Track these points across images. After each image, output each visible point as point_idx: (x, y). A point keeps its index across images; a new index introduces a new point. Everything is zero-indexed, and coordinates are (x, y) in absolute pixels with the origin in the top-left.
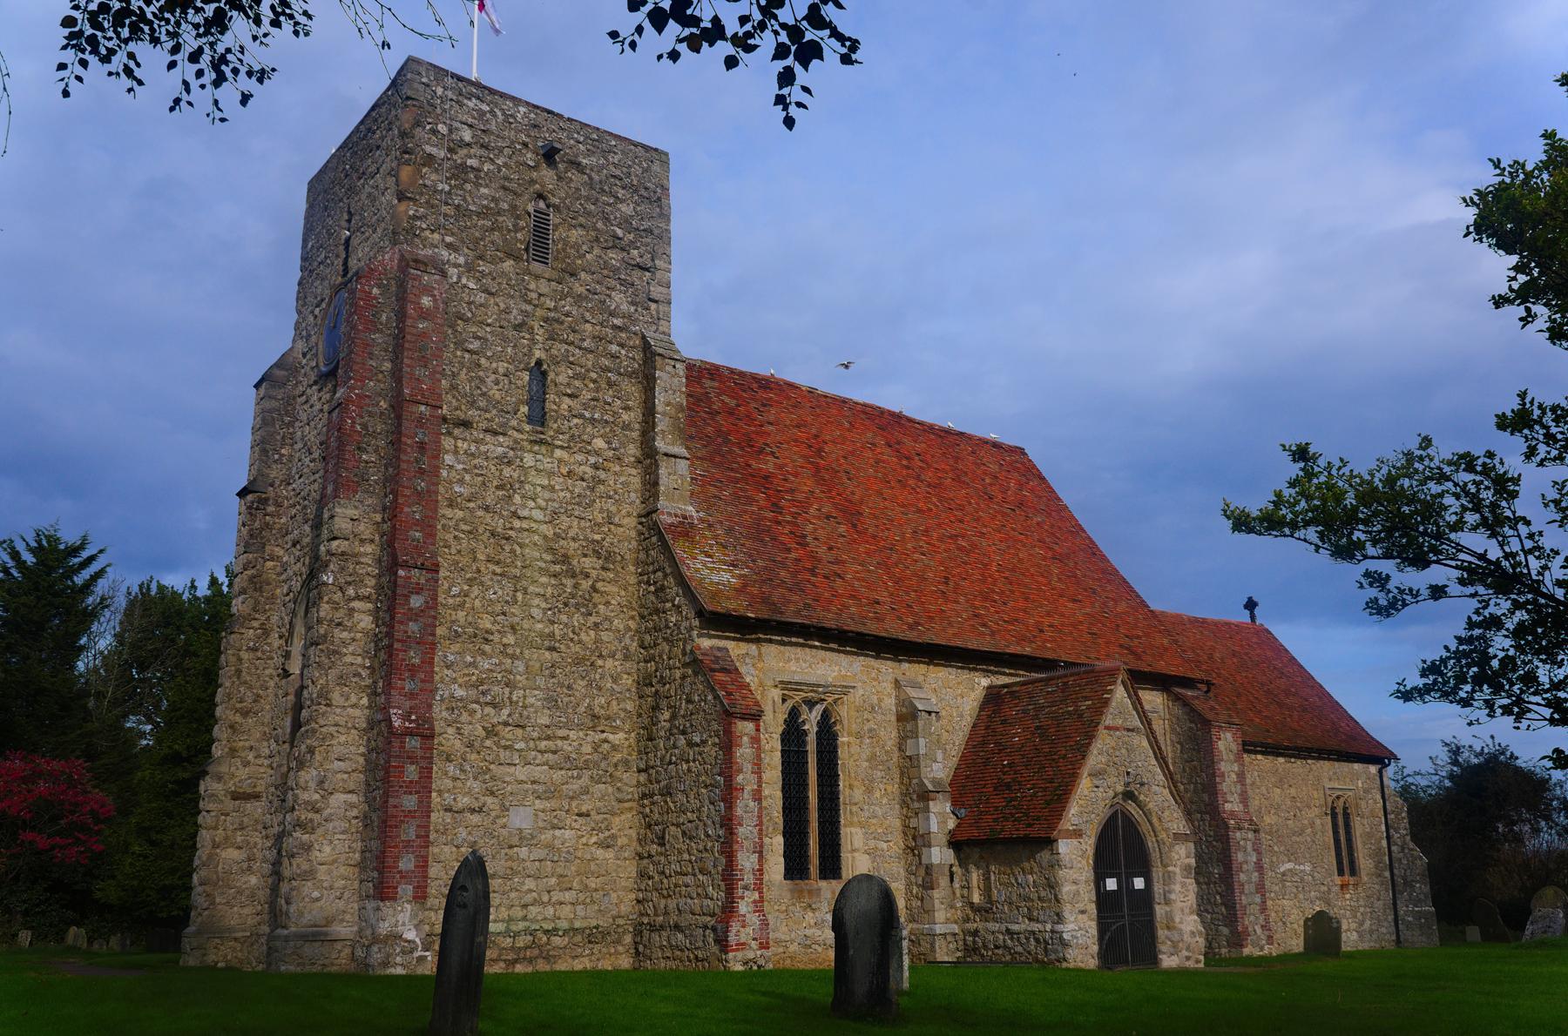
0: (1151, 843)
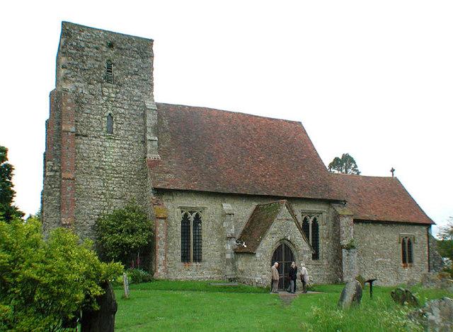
0: (295, 254)
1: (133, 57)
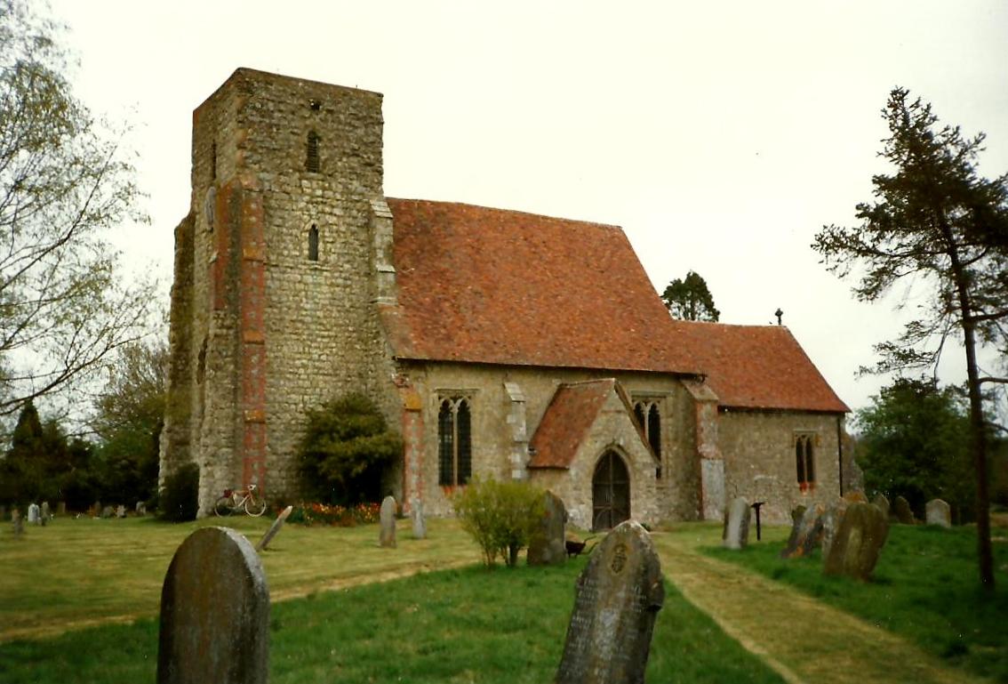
0: (630, 469)
1: (350, 124)
